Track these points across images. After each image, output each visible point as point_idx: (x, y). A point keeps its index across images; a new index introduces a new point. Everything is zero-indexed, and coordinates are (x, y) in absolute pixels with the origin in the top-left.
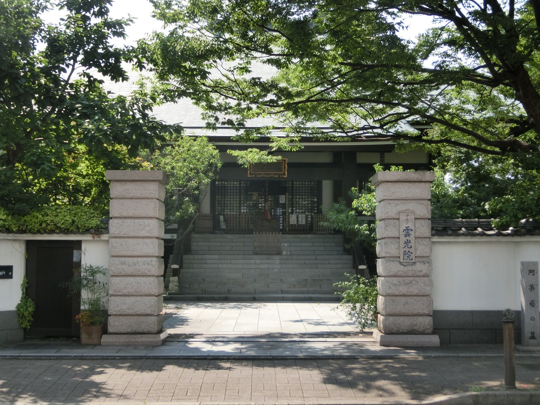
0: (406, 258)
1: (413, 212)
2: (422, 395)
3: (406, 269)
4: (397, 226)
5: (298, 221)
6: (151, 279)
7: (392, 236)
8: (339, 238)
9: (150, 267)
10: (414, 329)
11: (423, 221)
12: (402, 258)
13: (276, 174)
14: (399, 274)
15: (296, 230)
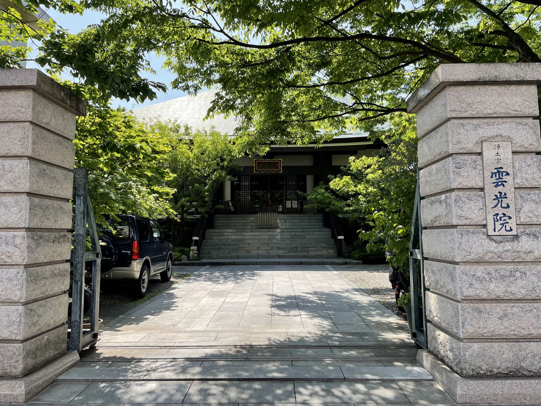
0: (498, 227)
1: (509, 139)
3: (500, 248)
4: (479, 167)
6: (13, 271)
7: (470, 185)
8: (320, 216)
9: (10, 249)
10: (522, 367)
11: (529, 157)
12: (490, 227)
14: (487, 258)
15: (291, 211)
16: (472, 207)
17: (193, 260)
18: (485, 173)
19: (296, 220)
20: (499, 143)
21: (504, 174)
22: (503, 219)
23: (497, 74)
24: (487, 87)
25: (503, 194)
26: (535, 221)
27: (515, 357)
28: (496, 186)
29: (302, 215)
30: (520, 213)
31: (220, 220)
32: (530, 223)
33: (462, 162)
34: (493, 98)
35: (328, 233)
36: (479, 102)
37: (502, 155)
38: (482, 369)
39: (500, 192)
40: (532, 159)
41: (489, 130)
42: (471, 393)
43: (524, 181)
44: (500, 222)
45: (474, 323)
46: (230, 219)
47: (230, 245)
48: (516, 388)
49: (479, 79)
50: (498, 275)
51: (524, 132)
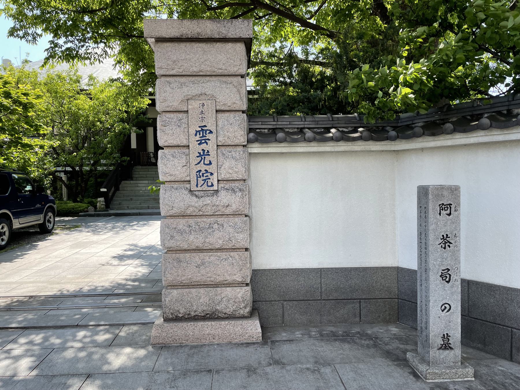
0: (201, 182)
1: (213, 98)
3: (200, 203)
7: (175, 143)
10: (216, 310)
11: (232, 115)
14: (188, 212)
16: (176, 164)
17: (100, 211)
18: (190, 131)
20: (204, 102)
21: (208, 132)
22: (205, 175)
23: (199, 30)
24: (193, 44)
25: (206, 151)
26: (235, 177)
27: (211, 301)
28: (199, 144)
30: (221, 169)
32: (231, 179)
33: (168, 120)
34: (198, 56)
36: (184, 60)
37: (206, 114)
38: (180, 313)
39: (203, 150)
40: (234, 118)
41: (193, 88)
42: (164, 334)
43: (226, 139)
44: (202, 178)
45: (173, 272)
46: (150, 170)
47: (143, 196)
48: (207, 329)
49: (182, 36)
50: (197, 227)
51: (227, 91)
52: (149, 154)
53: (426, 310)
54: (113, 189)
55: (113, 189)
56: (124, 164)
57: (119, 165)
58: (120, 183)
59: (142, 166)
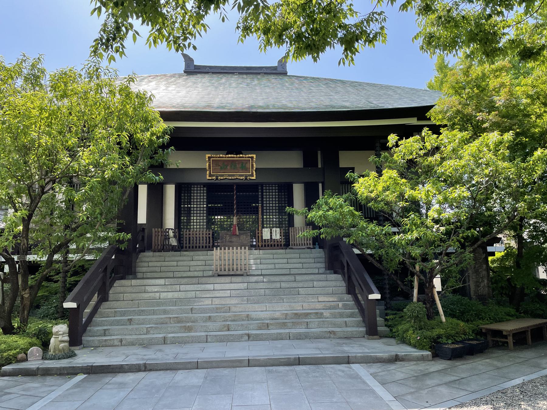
2: (281, 317)
5: (271, 236)
13: (242, 176)
15: (271, 245)
19: (280, 256)
29: (288, 251)
31: (148, 260)
35: (338, 284)
52: (167, 231)
53: (406, 385)
54: (95, 298)
55: (95, 298)
56: (123, 247)
57: (116, 249)
58: (111, 285)
59: (155, 251)
